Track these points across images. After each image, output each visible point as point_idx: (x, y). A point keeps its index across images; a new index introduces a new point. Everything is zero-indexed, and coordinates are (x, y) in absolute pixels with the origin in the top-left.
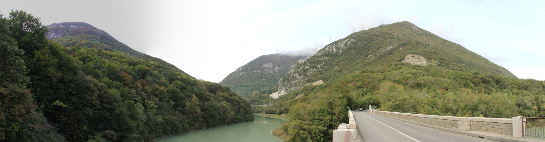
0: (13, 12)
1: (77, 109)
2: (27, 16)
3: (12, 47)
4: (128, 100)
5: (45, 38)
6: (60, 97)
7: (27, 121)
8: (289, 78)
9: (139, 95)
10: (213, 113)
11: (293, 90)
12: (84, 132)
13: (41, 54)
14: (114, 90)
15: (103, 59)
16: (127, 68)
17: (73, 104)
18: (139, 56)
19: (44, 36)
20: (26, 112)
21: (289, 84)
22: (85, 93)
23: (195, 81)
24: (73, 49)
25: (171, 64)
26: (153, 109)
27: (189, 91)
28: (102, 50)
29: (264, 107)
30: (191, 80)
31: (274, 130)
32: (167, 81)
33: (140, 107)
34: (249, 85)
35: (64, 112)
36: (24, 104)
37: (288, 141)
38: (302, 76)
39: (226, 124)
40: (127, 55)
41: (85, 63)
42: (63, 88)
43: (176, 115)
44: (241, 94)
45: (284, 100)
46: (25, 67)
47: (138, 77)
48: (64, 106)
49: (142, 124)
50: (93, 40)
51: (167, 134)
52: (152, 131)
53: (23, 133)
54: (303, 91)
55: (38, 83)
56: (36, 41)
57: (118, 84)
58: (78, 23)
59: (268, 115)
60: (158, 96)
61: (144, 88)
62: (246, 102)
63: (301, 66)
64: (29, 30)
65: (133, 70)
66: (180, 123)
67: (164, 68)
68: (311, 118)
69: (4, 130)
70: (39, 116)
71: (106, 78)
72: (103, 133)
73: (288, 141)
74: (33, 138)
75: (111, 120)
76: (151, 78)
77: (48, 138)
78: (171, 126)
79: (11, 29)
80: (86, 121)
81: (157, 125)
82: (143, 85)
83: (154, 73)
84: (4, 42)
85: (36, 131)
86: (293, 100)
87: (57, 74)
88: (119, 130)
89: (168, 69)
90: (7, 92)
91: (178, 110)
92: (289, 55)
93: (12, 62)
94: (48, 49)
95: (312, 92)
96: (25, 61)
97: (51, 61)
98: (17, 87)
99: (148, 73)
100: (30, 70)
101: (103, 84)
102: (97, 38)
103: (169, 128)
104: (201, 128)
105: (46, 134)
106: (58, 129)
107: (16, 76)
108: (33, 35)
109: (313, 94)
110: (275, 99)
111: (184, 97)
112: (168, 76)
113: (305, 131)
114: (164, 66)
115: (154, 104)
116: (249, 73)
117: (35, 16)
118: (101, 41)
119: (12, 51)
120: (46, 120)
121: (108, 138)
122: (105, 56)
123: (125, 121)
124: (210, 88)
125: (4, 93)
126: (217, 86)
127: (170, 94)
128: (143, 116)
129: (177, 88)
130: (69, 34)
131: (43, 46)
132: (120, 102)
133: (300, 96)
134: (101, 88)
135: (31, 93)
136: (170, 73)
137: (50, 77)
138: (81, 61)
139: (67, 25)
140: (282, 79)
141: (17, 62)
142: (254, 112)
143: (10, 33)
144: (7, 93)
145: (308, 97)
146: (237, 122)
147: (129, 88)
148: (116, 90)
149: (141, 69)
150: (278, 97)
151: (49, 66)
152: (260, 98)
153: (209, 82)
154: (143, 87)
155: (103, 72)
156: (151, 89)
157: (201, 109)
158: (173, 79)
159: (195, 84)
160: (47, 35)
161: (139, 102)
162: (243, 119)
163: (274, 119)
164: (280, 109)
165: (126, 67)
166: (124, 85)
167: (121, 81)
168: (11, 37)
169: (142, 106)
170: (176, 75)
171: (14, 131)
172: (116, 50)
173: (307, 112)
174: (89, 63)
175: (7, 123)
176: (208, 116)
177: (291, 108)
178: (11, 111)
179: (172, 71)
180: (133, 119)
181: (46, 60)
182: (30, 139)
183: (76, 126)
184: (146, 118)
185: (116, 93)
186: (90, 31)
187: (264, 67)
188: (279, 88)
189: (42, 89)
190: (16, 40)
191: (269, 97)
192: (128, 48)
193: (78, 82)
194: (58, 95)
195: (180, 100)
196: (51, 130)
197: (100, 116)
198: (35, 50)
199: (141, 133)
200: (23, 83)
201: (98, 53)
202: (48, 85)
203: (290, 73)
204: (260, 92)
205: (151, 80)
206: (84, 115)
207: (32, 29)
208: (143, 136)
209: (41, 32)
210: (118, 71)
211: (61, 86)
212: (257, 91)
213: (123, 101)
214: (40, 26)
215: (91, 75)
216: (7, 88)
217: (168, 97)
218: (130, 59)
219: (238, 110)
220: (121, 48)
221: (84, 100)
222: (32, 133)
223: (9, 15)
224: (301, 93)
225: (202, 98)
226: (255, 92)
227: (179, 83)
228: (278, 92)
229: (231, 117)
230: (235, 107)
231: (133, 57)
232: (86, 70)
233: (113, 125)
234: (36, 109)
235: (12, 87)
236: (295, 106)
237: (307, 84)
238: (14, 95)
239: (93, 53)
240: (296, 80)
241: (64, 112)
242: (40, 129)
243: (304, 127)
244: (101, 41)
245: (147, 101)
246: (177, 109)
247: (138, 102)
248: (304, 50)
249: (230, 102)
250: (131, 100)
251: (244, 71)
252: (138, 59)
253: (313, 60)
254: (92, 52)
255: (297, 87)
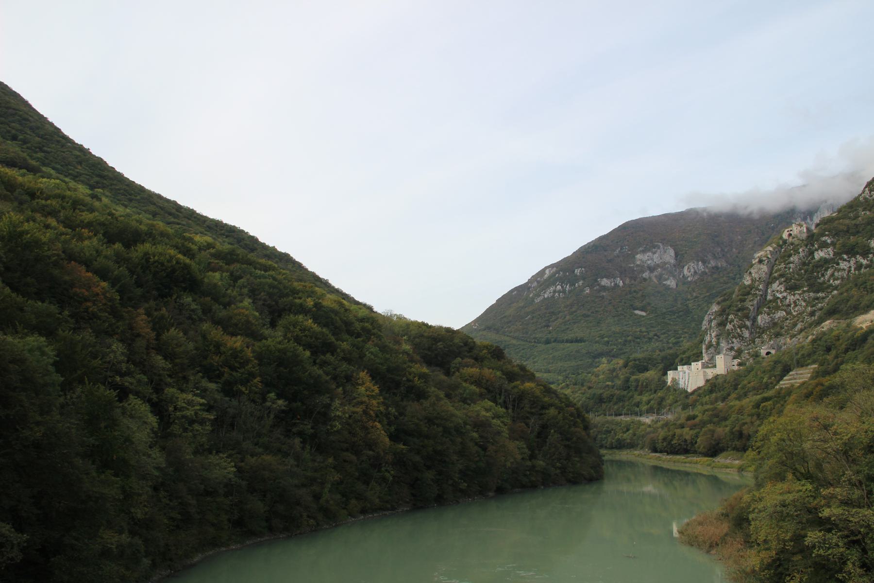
8: (748, 304)
10: (439, 448)
11: (768, 353)
14: (28, 339)
16: (97, 251)
18: (152, 208)
21: (747, 328)
23: (372, 317)
25: (279, 249)
27: (344, 359)
29: (644, 424)
30: (355, 316)
31: (686, 521)
33: (140, 418)
34: (579, 335)
37: (754, 571)
38: (804, 292)
39: (491, 494)
40: (100, 200)
44: (549, 372)
45: (729, 395)
47: (139, 291)
54: (809, 355)
59: (659, 458)
60: (220, 376)
62: (570, 404)
63: (797, 252)
65: (119, 259)
66: (304, 485)
67: (250, 263)
68: (858, 472)
73: (754, 571)
76: (194, 300)
82: (159, 326)
83: (206, 280)
86: (766, 395)
89: (266, 269)
91: (300, 434)
92: (743, 212)
95: (856, 358)
103: (258, 506)
104: (389, 506)
109: (860, 366)
110: (689, 390)
111: (326, 382)
113: (829, 531)
114: (252, 256)
115: (201, 405)
116: (582, 291)
124: (429, 349)
126: (456, 341)
129: (300, 344)
133: (800, 376)
136: (271, 286)
140: (715, 308)
142: (601, 447)
145: (836, 379)
146: (532, 487)
148: (34, 340)
149: (155, 262)
150: (701, 383)
152: (626, 386)
153: (426, 325)
154: (158, 336)
156: (191, 345)
157: (393, 429)
161: (137, 394)
162: (558, 471)
163: (687, 474)
164: (713, 432)
165: (90, 244)
169: (150, 415)
170: (294, 292)
172: (52, 172)
173: (834, 445)
176: (417, 458)
177: (763, 430)
179: (280, 277)
185: (37, 353)
187: (638, 263)
188: (704, 347)
191: (665, 382)
192: (106, 173)
195: (306, 392)
203: (747, 281)
204: (625, 366)
205: (194, 306)
212: (615, 361)
213: (66, 387)
217: (258, 379)
218: (111, 214)
219: (539, 435)
224: (801, 364)
225: (398, 384)
226: (604, 365)
227: (306, 323)
228: (700, 363)
229: (508, 464)
230: (527, 424)
231: (128, 210)
236: (782, 420)
237: (827, 324)
240: (777, 308)
243: (826, 513)
245: (170, 391)
246: (295, 430)
247: (131, 396)
248: (804, 186)
249: (505, 405)
250: (102, 388)
251: (562, 281)
252: (148, 222)
253: (847, 221)
255: (782, 340)
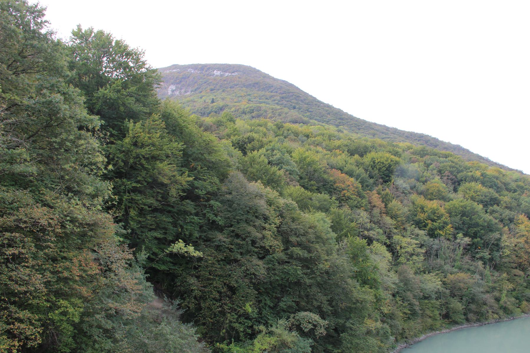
0: (80, 29)
1: (228, 261)
2: (113, 44)
3: (71, 108)
4: (351, 238)
5: (152, 95)
6: (187, 233)
7: (103, 293)
9: (377, 223)
12: (246, 318)
13: (141, 130)
15: (288, 144)
17: (218, 248)
18: (372, 131)
19: (152, 90)
20: (101, 270)
22: (247, 221)
23: (523, 178)
24: (218, 122)
26: (414, 257)
27: (506, 207)
28: (285, 123)
32: (444, 185)
33: (381, 254)
35: (195, 268)
36: (95, 251)
40: (342, 132)
41: (245, 154)
42: (193, 211)
43: (475, 272)
46: (100, 159)
47: (371, 181)
48: (197, 254)
49: (386, 296)
50: (264, 103)
51: (456, 323)
52: (414, 313)
53: (91, 326)
55: (134, 197)
56: (131, 101)
57: (325, 200)
58: (229, 66)
61: (390, 205)
64: (115, 73)
66: (488, 292)
69: (40, 320)
70: (135, 281)
71: (294, 186)
72: (291, 320)
74: (117, 336)
75: (310, 286)
77: (157, 334)
78: (464, 299)
79: (72, 66)
80: (250, 291)
81: (425, 298)
82: (386, 200)
83: (410, 169)
84: (51, 93)
85: (124, 318)
87: (179, 178)
88: (331, 310)
89: (446, 157)
90: (52, 219)
91: (481, 258)
93: (68, 144)
94: (160, 119)
96: (102, 144)
97: (165, 147)
98: (77, 207)
99: (395, 170)
100: (114, 165)
101: (290, 201)
102: (272, 96)
103: (457, 305)
105: (151, 325)
106: (181, 312)
107: (77, 180)
108: (125, 86)
111: (496, 224)
112: (447, 173)
114: (436, 150)
117: (132, 45)
118: (281, 103)
119: (71, 117)
120: (152, 289)
121: (304, 332)
122: (292, 136)
123: (343, 289)
125: (44, 222)
127: (457, 219)
128: (388, 276)
130: (209, 88)
131: (148, 111)
132: (331, 241)
134: (284, 211)
135: (115, 222)
136: (451, 167)
137: (163, 185)
138: (237, 149)
139: (206, 68)
141: (82, 145)
143: (68, 76)
144: (51, 221)
147: (352, 208)
148: (320, 215)
151: (160, 160)
155: (288, 172)
156: (406, 209)
158: (459, 178)
159: (522, 187)
160: (158, 90)
161: (378, 240)
165: (341, 158)
166: (340, 202)
167: (330, 193)
168: (71, 85)
170: (467, 168)
171: (68, 320)
172: (316, 122)
174: (256, 152)
175: (47, 301)
178: (60, 269)
179: (455, 160)
180: (364, 282)
181: (153, 145)
182: (109, 340)
183: (225, 304)
184: (397, 282)
186: (257, 83)
189: (141, 212)
190: (84, 92)
193: (229, 197)
194: (182, 227)
195: (482, 231)
196: (164, 315)
197: (284, 277)
198: (129, 121)
199: (386, 318)
200: (93, 196)
201: (276, 130)
202: (158, 203)
205: (404, 185)
206: (245, 276)
207: (122, 73)
208: (391, 326)
209: (144, 81)
210: (323, 169)
211: (189, 206)
213: (339, 240)
214: (142, 68)
215: (259, 181)
216: (51, 207)
217: (450, 225)
218: (350, 139)
220: (329, 117)
221: (244, 239)
222: (115, 325)
223: (71, 35)
227: (477, 187)
232: (249, 169)
233: (316, 300)
234: (127, 263)
235: (65, 205)
238: (69, 226)
239: (265, 130)
241: (195, 268)
242: (137, 312)
244: (281, 103)
246: (478, 256)
247: (374, 242)
250: (358, 238)
254: (261, 129)
